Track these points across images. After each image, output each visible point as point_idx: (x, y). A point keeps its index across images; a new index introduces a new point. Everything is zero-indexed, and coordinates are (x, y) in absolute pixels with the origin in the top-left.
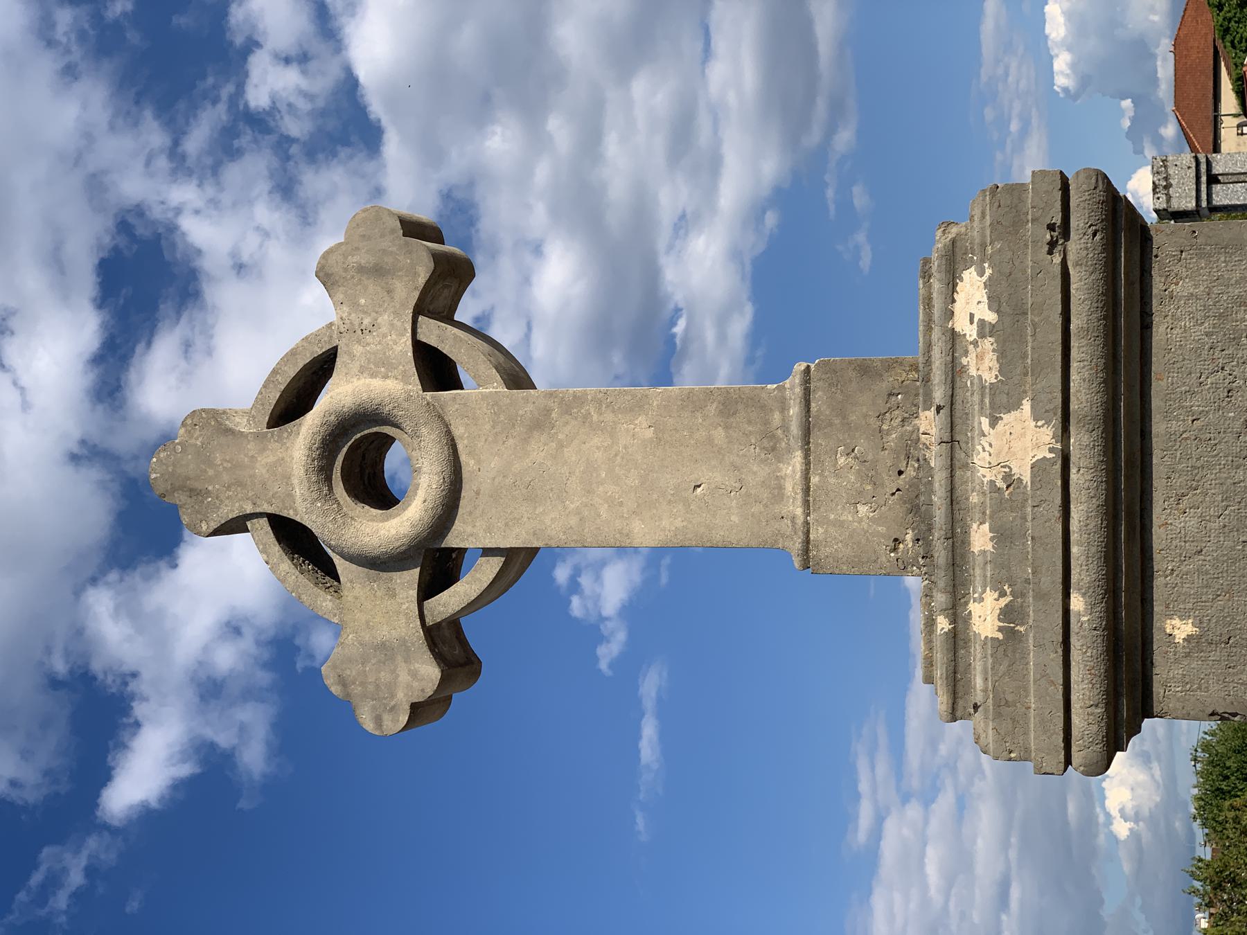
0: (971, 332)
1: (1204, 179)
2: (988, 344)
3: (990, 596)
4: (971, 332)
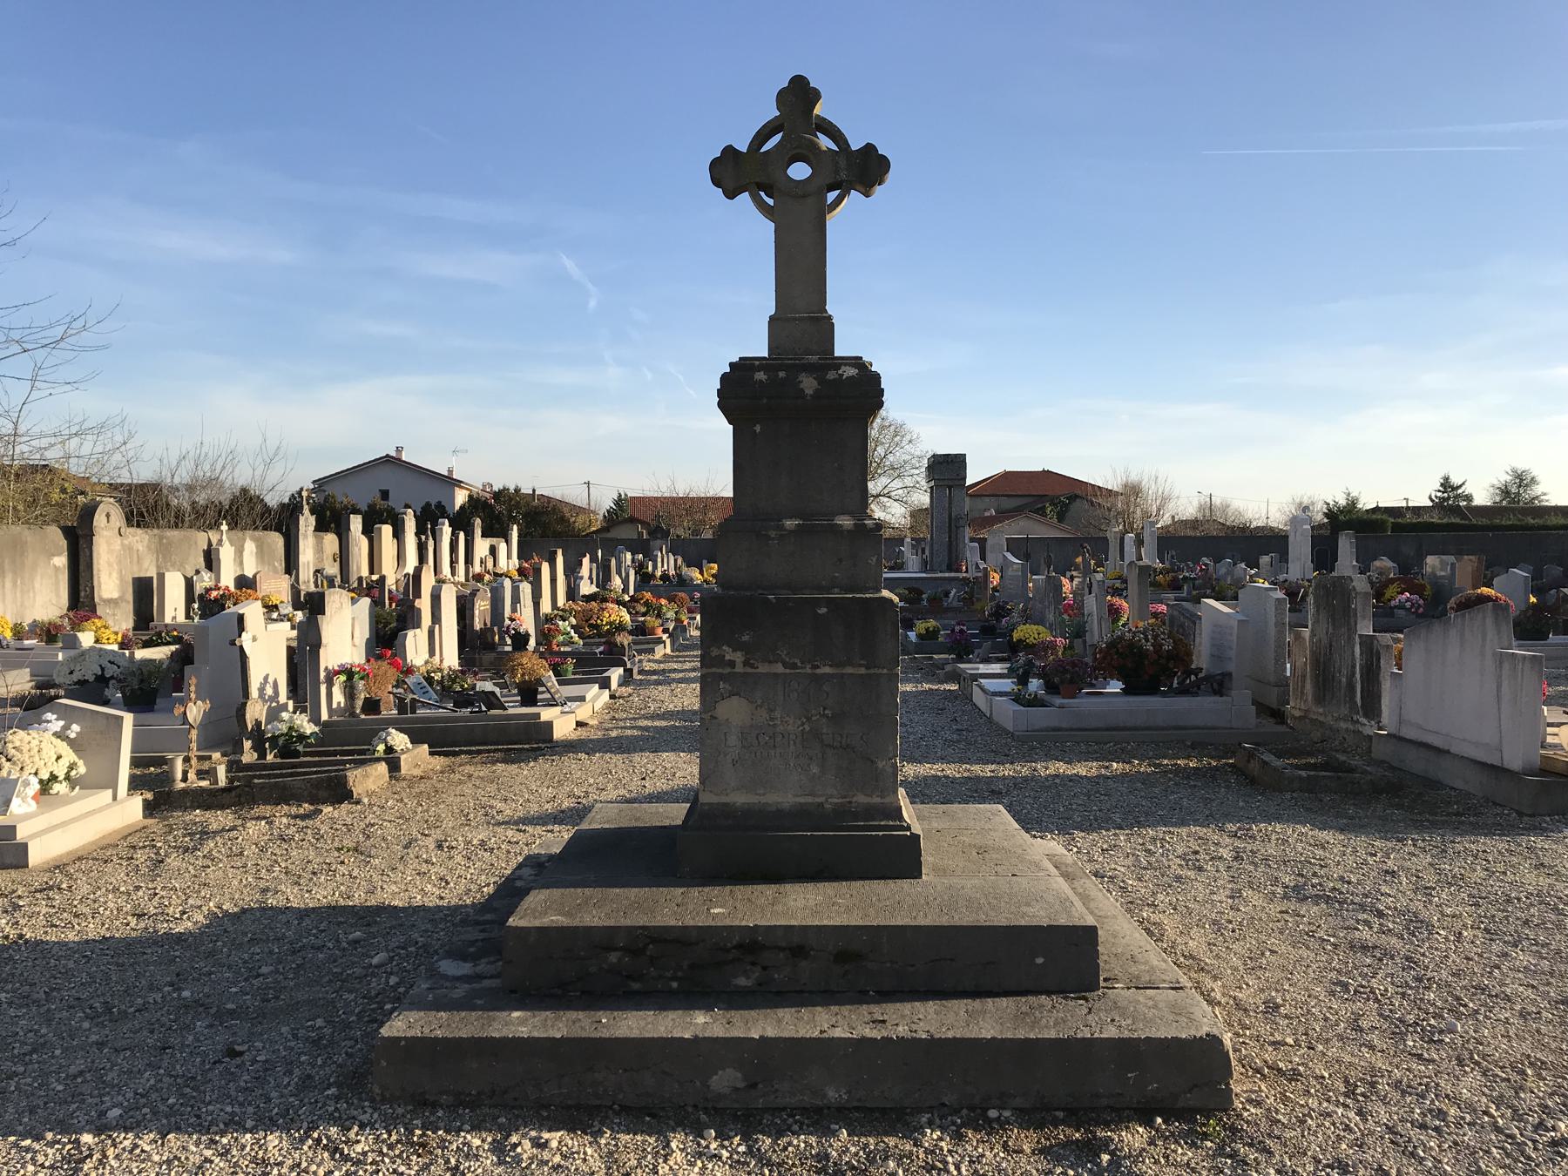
0: (840, 372)
1: (951, 483)
2: (837, 376)
3: (766, 377)
4: (840, 372)
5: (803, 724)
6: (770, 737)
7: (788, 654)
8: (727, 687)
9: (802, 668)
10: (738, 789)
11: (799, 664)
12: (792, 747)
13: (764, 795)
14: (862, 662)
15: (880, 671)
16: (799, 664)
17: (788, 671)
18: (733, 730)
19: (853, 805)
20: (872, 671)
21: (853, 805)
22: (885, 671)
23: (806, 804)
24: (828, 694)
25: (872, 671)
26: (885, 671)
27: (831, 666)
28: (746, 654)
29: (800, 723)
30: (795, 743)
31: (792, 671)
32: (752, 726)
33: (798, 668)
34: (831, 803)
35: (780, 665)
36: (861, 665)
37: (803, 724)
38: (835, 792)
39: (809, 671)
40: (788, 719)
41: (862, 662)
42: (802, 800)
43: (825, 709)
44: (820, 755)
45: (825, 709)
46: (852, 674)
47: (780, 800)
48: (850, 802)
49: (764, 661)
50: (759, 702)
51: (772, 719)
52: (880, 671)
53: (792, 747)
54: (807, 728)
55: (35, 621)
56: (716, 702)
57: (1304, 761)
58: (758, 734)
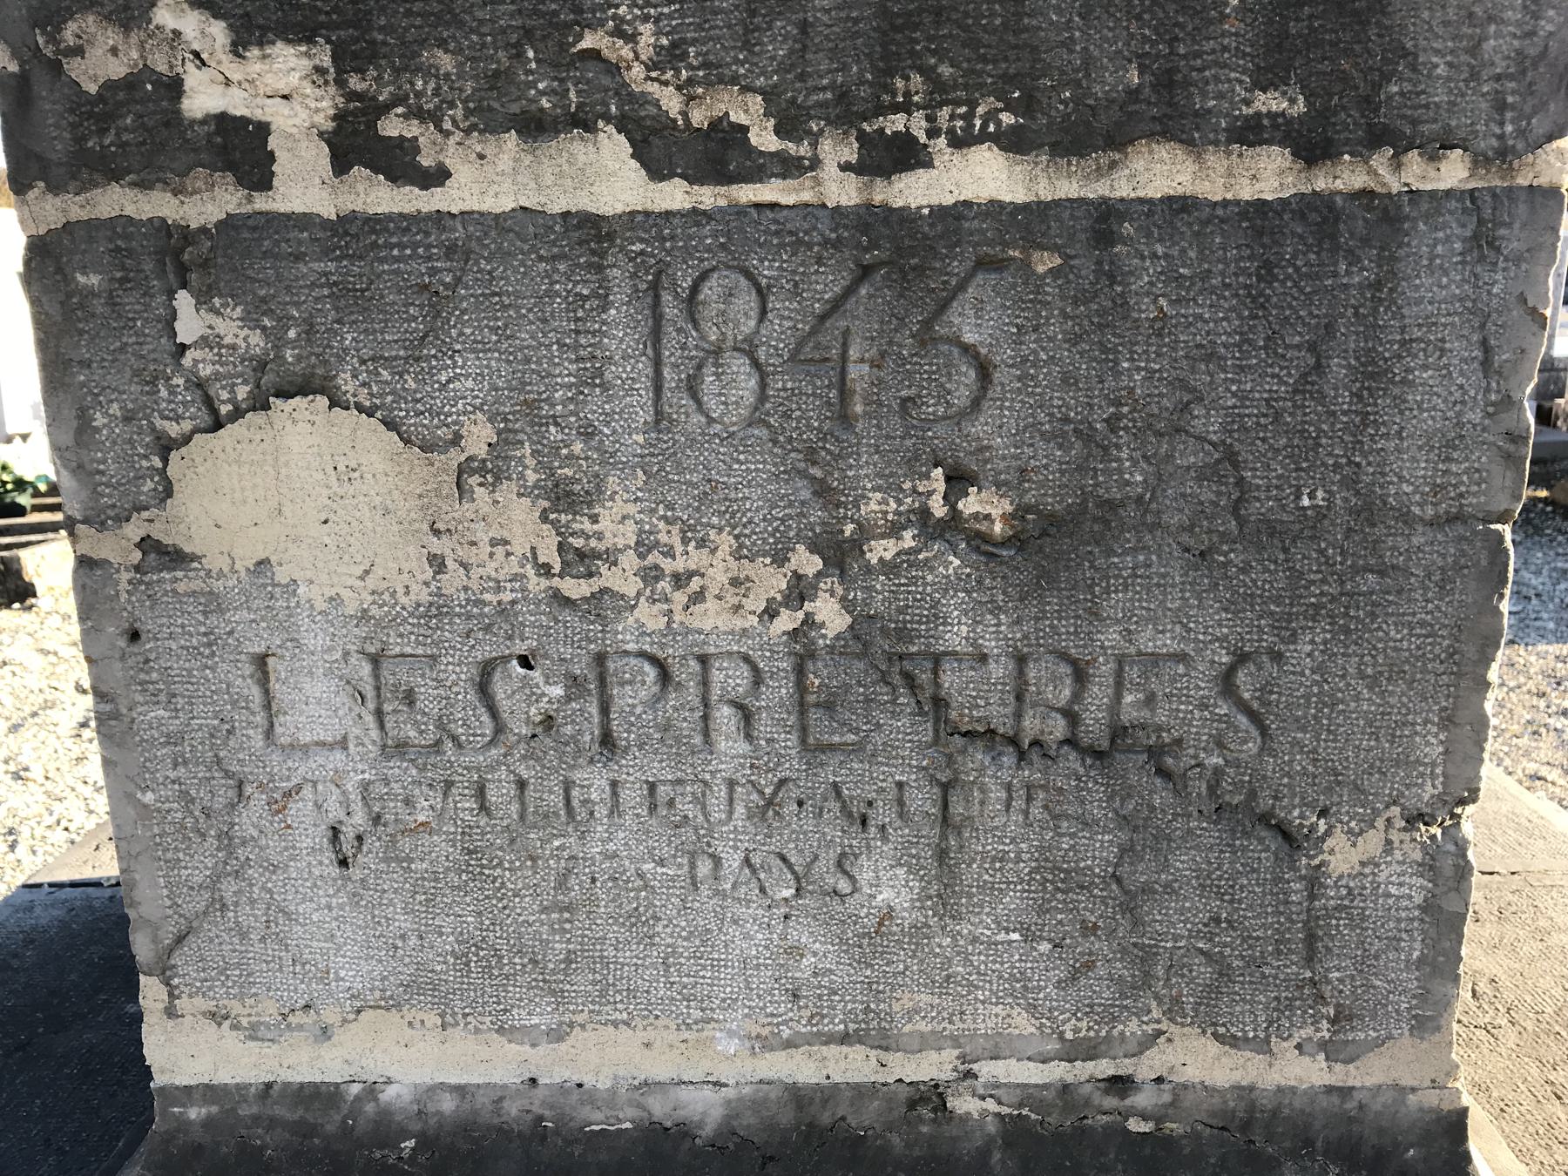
5: (800, 591)
6: (575, 684)
7: (668, 58)
8: (230, 328)
9: (789, 167)
10: (391, 1004)
11: (765, 139)
12: (730, 745)
13: (557, 1035)
14: (1270, 102)
15: (1416, 173)
16: (765, 139)
17: (675, 195)
18: (315, 640)
19: (1143, 1099)
20: (1346, 177)
21: (1143, 1099)
22: (1453, 172)
23: (828, 1093)
24: (985, 372)
25: (1346, 177)
26: (1453, 172)
27: (1014, 143)
28: (347, 60)
29: (774, 582)
30: (747, 716)
31: (708, 197)
32: (437, 611)
33: (758, 168)
34: (993, 1090)
35: (613, 148)
36: (1251, 133)
37: (800, 591)
38: (1023, 1024)
39: (842, 191)
40: (695, 558)
41: (1270, 102)
42: (803, 1068)
43: (959, 480)
44: (922, 799)
45: (959, 480)
46: (1180, 206)
47: (662, 1072)
48: (1120, 1084)
49: (486, 121)
50: (479, 437)
51: (581, 560)
52: (1416, 173)
53: (730, 745)
54: (830, 614)
55: (632, 156)
56: (166, 447)
57: (747, 193)
58: (487, 670)
